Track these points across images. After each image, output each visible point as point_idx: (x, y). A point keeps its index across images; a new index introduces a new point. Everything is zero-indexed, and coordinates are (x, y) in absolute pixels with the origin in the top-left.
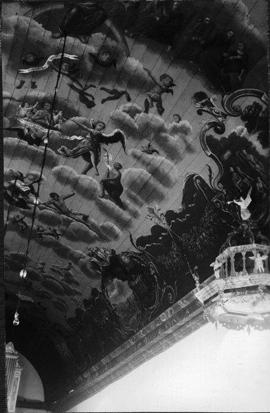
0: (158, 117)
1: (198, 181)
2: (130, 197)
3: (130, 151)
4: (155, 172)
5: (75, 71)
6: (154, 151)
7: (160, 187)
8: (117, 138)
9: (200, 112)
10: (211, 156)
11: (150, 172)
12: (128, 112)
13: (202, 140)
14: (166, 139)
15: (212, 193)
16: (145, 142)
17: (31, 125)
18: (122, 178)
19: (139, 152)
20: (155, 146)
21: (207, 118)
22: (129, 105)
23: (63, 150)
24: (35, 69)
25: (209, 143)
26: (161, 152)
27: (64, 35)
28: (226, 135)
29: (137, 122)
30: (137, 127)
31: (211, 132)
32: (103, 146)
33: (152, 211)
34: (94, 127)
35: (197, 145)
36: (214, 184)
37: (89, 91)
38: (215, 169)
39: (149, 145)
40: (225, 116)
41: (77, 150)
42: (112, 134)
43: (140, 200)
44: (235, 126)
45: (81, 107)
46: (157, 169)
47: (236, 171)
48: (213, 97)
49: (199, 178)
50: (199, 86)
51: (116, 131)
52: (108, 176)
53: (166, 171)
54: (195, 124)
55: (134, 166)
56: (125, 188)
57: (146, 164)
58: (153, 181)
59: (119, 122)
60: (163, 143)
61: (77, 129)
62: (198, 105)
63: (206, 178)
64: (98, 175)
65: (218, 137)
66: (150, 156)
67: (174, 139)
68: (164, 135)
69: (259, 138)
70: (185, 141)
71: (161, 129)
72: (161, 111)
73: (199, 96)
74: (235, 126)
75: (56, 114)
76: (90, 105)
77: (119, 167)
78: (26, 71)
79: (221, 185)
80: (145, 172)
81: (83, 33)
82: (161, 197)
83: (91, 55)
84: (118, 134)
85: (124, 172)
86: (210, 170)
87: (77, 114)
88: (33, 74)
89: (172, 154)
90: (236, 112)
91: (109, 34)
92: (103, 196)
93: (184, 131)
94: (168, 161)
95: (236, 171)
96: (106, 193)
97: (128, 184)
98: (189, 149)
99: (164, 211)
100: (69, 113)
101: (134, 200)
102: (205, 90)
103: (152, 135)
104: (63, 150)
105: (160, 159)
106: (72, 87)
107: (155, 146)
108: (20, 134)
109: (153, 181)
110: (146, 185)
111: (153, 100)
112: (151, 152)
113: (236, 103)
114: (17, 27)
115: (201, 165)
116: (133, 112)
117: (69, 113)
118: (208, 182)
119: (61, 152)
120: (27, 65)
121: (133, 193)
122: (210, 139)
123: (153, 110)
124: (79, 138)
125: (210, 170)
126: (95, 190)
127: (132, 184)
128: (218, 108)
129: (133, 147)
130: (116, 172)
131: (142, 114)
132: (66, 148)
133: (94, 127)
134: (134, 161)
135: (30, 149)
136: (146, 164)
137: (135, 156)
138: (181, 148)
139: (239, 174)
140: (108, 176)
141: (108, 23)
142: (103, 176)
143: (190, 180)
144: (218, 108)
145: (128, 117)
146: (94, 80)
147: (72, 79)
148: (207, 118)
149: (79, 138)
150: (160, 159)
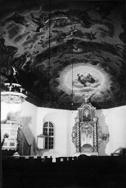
0: (37, 42)
1: (16, 51)
2: (13, 25)
3: (31, 32)
4: (20, 37)
5: (65, 35)
6: (28, 39)
7: (15, 38)
8: (38, 30)
9: (34, 52)
10: (22, 54)
11: (21, 35)
12: (43, 37)
13: (27, 52)
14: (30, 43)
15: (12, 56)
16: (32, 37)
17: (65, 18)
18: (22, 25)
19: (30, 34)
20: (29, 39)
21: (32, 53)
22: (45, 38)
23: (46, 15)
24: (73, 32)
25: (26, 54)
26: (27, 41)
27: (73, 39)
28: (27, 58)
29: (40, 38)
30: (38, 37)
31: (28, 54)
32: (38, 26)
33: (5, 33)
34: (46, 28)
35: (26, 51)
36: (15, 56)
37: (57, 33)
38: (19, 56)
39: (30, 38)
40: (31, 57)
41: (42, 19)
42: (40, 30)
43: (10, 29)
44: (28, 59)
45: (54, 29)
46: (17, 33)
47: (18, 62)
48: (36, 55)
49: (17, 51)
50: (40, 52)
51: (40, 32)
52: (25, 21)
53: (20, 41)
54: (31, 51)
55: (25, 31)
56: (17, 24)
57: (24, 35)
58: (17, 36)
59: (42, 33)
60: (30, 42)
61: (50, 24)
62: (36, 52)
63: (17, 53)
64: (28, 18)
65: (27, 55)
66: (27, 37)
67: (30, 45)
68: (32, 43)
69: (25, 65)
70: (28, 48)
71: (34, 42)
72: (38, 43)
73: (38, 52)
74: (28, 59)
75: (59, 24)
76: (53, 31)
77: (27, 26)
78: (75, 31)
79: (14, 58)
80: (21, 34)
81: (68, 41)
82: (11, 37)
83: (64, 39)
84: (39, 31)
85: (24, 27)
86: (19, 55)
87: (54, 27)
88: (73, 30)
89: (25, 44)
90: (31, 59)
91: (64, 43)
92: (16, 14)
93: (31, 48)
94: (23, 42)
95: (18, 62)
96: (17, 16)
97: (18, 26)
98: (26, 48)
99: (4, 38)
100: (56, 26)
101: (10, 26)
102: (39, 53)
103: (33, 40)
104: (46, 15)
105: (25, 40)
106: (62, 32)
107: (29, 39)
108: (64, 14)
109: (17, 36)
110: (16, 33)
111: (42, 43)
112: (28, 38)
113: (33, 59)
114: (84, 38)
115: (20, 52)
116: (42, 37)
117: (56, 26)
118: (15, 54)
119: (46, 14)
120: (76, 32)
121: (13, 27)
122: (27, 54)
123: (40, 42)
124: (46, 22)
125: (19, 55)
126: (21, 13)
127: (18, 28)
128: (33, 55)
129: (32, 34)
130: (25, 24)
131: (41, 39)
132: (46, 16)
133: (46, 28)
134: (27, 31)
135: (56, 10)
136: (24, 35)
137: (28, 33)
138: (26, 46)
139: (18, 63)
140: (25, 21)
141: (66, 44)
142: (26, 19)
143: (16, 49)
144: (33, 55)
145: (42, 36)
146: (58, 36)
147: (63, 33)
148: (32, 53)
149: (46, 22)
150: (25, 40)
